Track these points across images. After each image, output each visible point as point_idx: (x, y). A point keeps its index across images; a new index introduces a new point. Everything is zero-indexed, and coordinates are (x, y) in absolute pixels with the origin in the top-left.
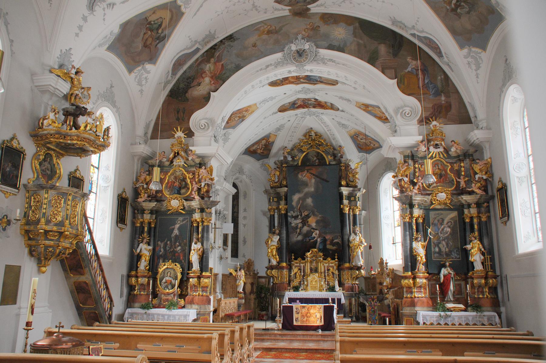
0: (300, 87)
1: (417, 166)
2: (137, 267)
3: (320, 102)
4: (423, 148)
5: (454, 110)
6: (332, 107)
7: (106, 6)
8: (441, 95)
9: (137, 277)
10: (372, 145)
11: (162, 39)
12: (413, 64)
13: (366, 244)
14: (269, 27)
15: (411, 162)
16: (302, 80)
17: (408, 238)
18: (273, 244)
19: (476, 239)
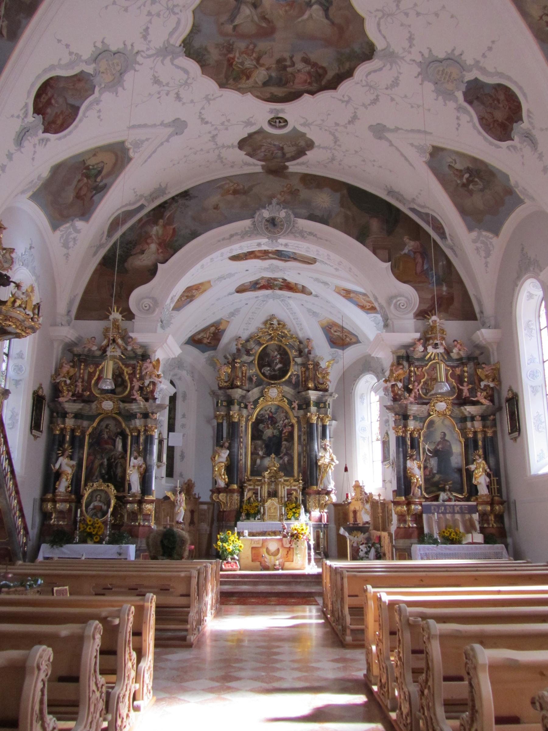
0: (267, 263)
1: (412, 369)
2: (55, 489)
3: (289, 283)
4: (421, 348)
5: (456, 304)
6: (304, 290)
7: (37, 142)
8: (442, 285)
9: (54, 501)
10: (348, 339)
11: (101, 189)
12: (410, 245)
13: (337, 462)
14: (235, 186)
15: (405, 364)
16: (270, 255)
17: (401, 455)
18: (221, 460)
19: (480, 458)
